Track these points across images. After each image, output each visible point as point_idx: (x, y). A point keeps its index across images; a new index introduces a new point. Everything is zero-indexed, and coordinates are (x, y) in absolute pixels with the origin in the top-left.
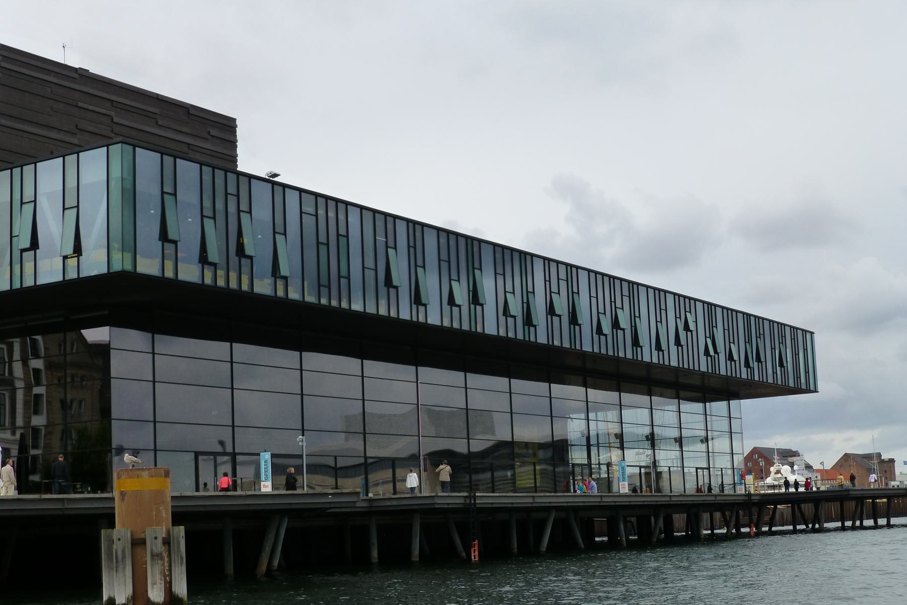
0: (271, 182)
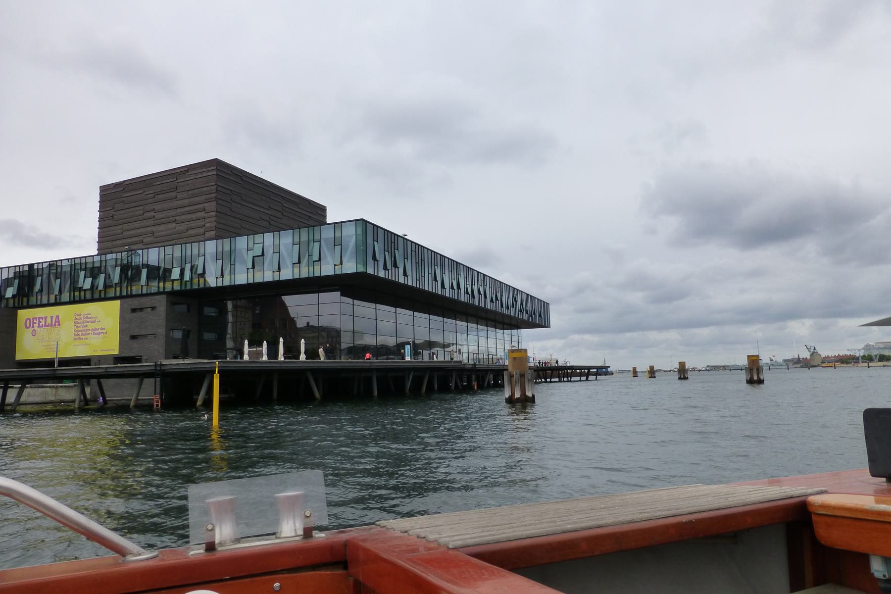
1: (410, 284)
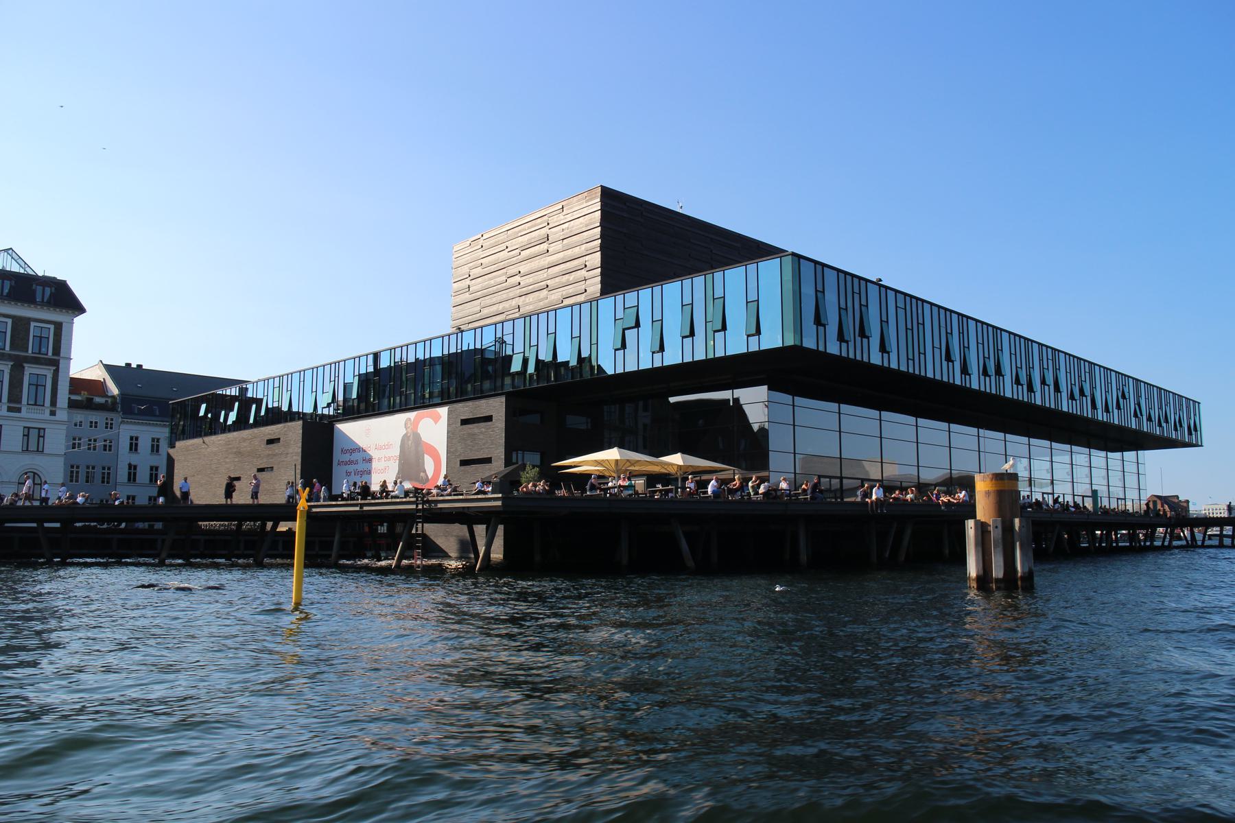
0: (878, 283)
1: (894, 365)
